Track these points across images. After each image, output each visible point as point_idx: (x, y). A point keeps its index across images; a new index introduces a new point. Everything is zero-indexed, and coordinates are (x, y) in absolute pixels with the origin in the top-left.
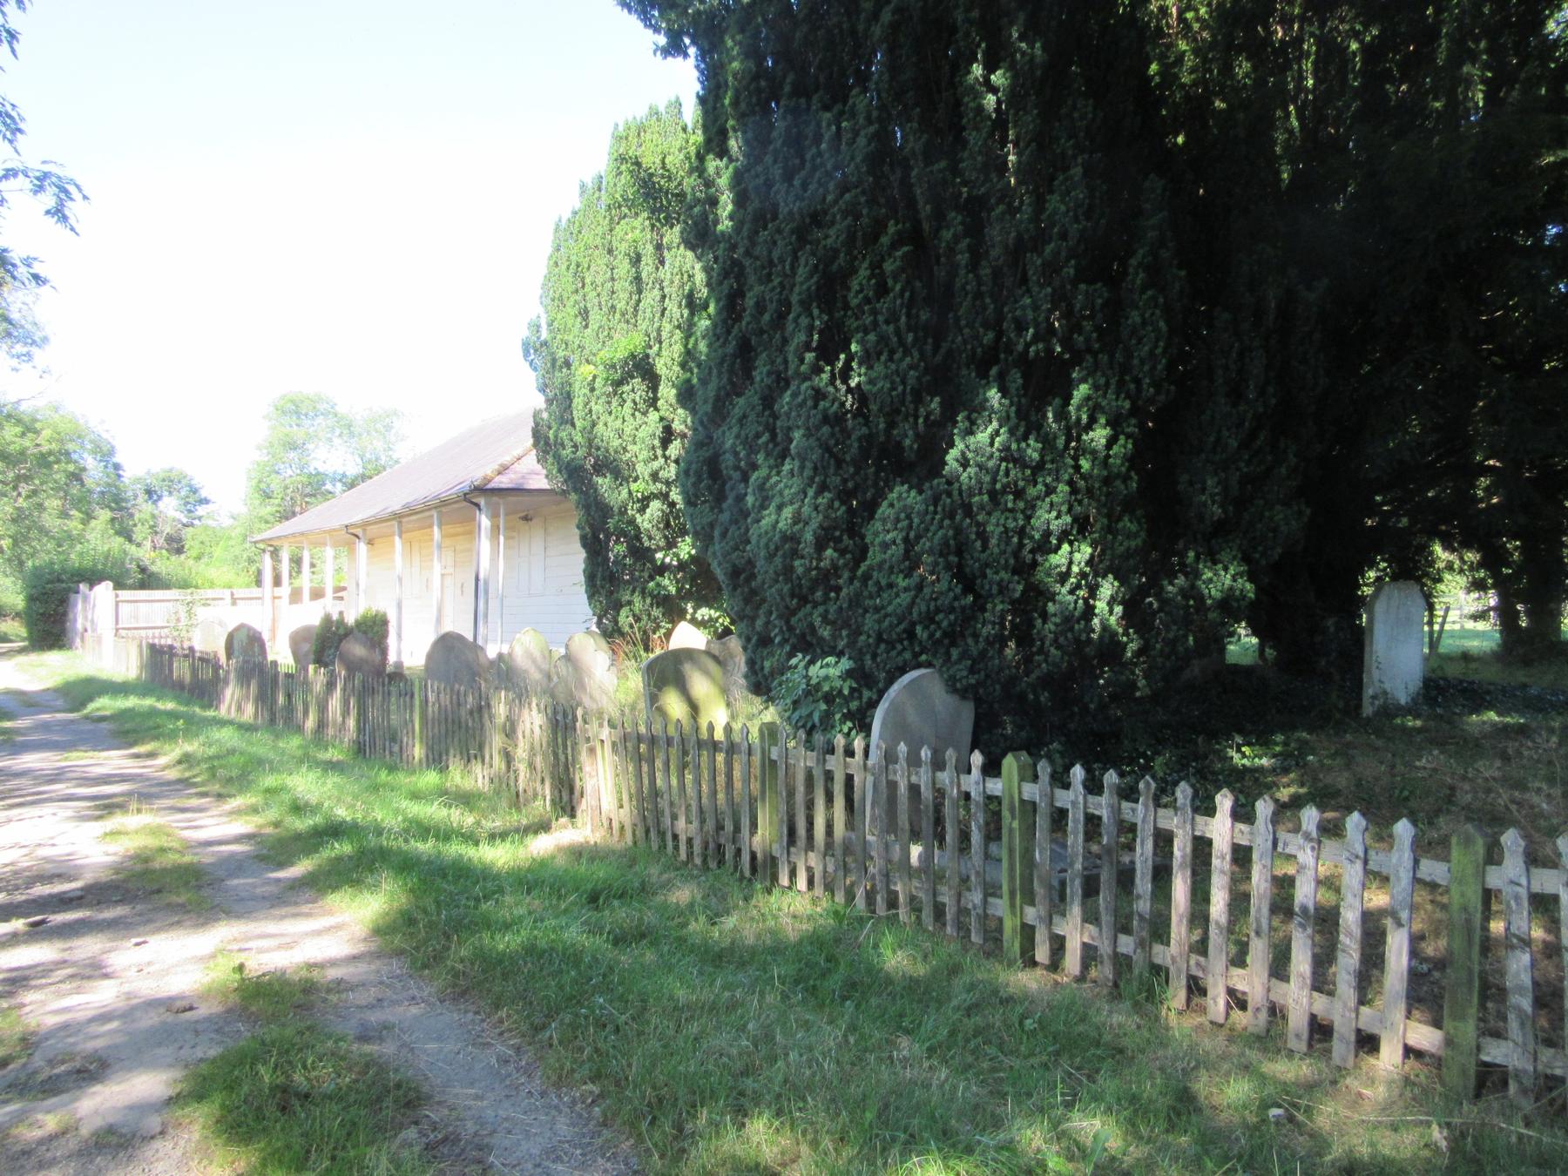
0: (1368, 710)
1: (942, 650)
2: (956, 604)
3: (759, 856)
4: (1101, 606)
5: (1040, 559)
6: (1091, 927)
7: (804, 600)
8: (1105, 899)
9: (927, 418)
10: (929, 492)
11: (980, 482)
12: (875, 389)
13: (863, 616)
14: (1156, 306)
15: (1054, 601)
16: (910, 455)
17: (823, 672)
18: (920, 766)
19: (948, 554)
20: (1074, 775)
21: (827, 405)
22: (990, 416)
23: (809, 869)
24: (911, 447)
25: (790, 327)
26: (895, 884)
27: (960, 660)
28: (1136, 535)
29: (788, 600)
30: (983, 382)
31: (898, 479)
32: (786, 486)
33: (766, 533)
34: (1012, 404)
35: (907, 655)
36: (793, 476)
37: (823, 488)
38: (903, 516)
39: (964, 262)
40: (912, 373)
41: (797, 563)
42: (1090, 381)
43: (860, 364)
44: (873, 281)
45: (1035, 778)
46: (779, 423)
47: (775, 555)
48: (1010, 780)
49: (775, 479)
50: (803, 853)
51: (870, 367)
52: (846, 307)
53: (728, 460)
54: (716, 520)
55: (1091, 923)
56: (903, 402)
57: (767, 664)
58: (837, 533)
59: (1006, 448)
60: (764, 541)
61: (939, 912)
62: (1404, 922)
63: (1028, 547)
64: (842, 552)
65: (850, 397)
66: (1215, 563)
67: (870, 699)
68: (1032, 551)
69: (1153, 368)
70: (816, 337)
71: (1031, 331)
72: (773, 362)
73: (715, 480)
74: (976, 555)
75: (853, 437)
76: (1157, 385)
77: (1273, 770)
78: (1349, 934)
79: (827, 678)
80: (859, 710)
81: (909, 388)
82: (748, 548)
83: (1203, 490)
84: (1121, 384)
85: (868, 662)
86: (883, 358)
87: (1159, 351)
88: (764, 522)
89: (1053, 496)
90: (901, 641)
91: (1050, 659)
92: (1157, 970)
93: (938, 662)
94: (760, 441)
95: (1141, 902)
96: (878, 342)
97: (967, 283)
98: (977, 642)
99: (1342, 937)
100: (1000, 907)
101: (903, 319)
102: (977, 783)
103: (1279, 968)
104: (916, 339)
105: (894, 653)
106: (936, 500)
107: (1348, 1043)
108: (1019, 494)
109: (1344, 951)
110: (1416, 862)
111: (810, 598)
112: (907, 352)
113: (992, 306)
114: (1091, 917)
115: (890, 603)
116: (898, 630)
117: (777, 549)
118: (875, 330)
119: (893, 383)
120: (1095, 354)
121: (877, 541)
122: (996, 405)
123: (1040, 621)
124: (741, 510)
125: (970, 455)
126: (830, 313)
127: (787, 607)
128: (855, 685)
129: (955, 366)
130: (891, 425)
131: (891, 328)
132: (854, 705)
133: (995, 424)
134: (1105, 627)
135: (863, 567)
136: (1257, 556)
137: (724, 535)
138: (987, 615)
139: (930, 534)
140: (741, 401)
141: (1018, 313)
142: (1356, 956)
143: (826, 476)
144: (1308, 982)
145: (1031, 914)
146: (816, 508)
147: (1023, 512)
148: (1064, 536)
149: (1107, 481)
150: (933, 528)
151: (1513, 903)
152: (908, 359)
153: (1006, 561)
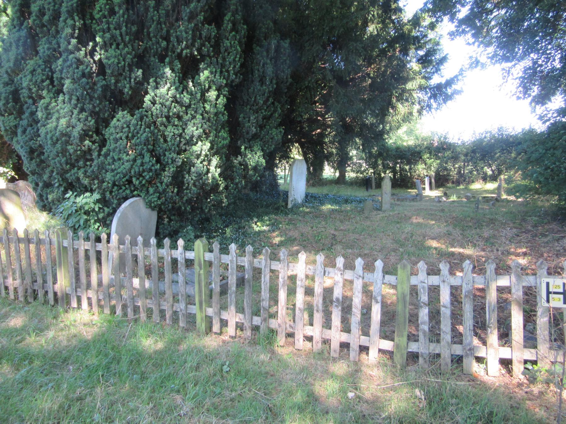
0: (290, 206)
1: (145, 189)
2: (153, 168)
3: (59, 294)
4: (212, 169)
5: (188, 148)
6: (240, 315)
7: (73, 166)
8: (247, 302)
9: (135, 79)
10: (138, 115)
11: (161, 111)
12: (109, 63)
13: (105, 173)
14: (236, 39)
15: (194, 167)
16: (126, 97)
17: (84, 201)
18: (150, 247)
19: (149, 144)
20: (231, 248)
21: (85, 68)
22: (166, 81)
23: (89, 299)
24: (128, 93)
25: (61, 24)
26: (138, 302)
27: (154, 193)
28: (226, 139)
29: (64, 166)
30: (162, 64)
31: (120, 108)
32: (61, 108)
33: (51, 132)
34: (176, 76)
35: (128, 192)
36: (64, 103)
37: (82, 110)
38: (125, 126)
39: (152, 5)
40: (129, 56)
41: (69, 147)
42: (209, 69)
43: (101, 49)
44: (108, 7)
45: (211, 251)
46: (55, 76)
47: (57, 143)
48: (199, 252)
49: (54, 104)
50: (85, 291)
51: (106, 51)
52: (92, 18)
53: (24, 93)
54: (19, 124)
55: (240, 313)
56: (124, 71)
57: (50, 197)
58: (91, 133)
59: (174, 97)
60: (49, 136)
61: (162, 313)
62: (379, 301)
63: (183, 143)
64: (94, 142)
65: (94, 65)
66: (252, 151)
67: (109, 212)
68: (185, 144)
69: (235, 67)
70: (77, 31)
71: (185, 43)
72: (50, 43)
73: (16, 103)
74: (161, 145)
75: (98, 85)
76: (236, 74)
77: (269, 231)
78: (357, 308)
79: (86, 203)
80: (103, 218)
81: (127, 63)
82: (39, 139)
83: (249, 121)
84: (221, 72)
85: (108, 195)
86: (113, 47)
87: (237, 59)
88: (49, 126)
89: (195, 120)
90: (125, 185)
91: (192, 192)
92: (273, 332)
93: (143, 195)
94: (45, 84)
95: (264, 303)
96: (111, 39)
97: (154, 16)
98: (162, 185)
99: (353, 309)
100: (194, 309)
101: (124, 28)
102: (181, 254)
103: (327, 324)
104: (130, 40)
105: (121, 191)
106: (141, 119)
107: (356, 351)
108: (179, 118)
109: (354, 315)
110: (384, 276)
111: (76, 164)
112: (126, 46)
113: (165, 29)
114: (240, 310)
115: (119, 167)
116: (123, 180)
117: (58, 140)
118: (109, 32)
119: (119, 60)
120: (210, 58)
121: (111, 138)
122: (169, 76)
123: (187, 175)
124: (34, 120)
125: (157, 99)
126: (84, 20)
127: (62, 169)
128: (101, 206)
129: (148, 55)
130: (117, 82)
131: (118, 32)
132: (101, 216)
133: (169, 85)
134: (214, 178)
135: (104, 150)
136: (266, 148)
137: (24, 132)
138: (166, 173)
139: (139, 135)
140: (32, 62)
141: (178, 33)
142: (359, 316)
143: (84, 104)
144: (339, 329)
145: (210, 311)
146: (79, 120)
147: (181, 126)
148: (199, 138)
149: (216, 114)
150: (141, 132)
151: (422, 290)
152: (126, 49)
153: (175, 148)
